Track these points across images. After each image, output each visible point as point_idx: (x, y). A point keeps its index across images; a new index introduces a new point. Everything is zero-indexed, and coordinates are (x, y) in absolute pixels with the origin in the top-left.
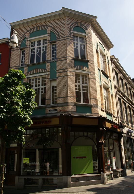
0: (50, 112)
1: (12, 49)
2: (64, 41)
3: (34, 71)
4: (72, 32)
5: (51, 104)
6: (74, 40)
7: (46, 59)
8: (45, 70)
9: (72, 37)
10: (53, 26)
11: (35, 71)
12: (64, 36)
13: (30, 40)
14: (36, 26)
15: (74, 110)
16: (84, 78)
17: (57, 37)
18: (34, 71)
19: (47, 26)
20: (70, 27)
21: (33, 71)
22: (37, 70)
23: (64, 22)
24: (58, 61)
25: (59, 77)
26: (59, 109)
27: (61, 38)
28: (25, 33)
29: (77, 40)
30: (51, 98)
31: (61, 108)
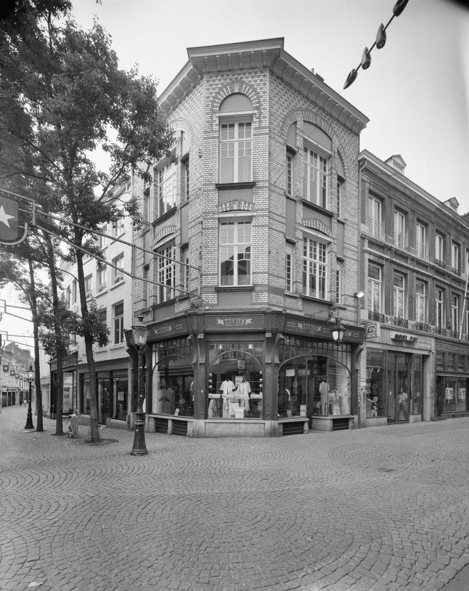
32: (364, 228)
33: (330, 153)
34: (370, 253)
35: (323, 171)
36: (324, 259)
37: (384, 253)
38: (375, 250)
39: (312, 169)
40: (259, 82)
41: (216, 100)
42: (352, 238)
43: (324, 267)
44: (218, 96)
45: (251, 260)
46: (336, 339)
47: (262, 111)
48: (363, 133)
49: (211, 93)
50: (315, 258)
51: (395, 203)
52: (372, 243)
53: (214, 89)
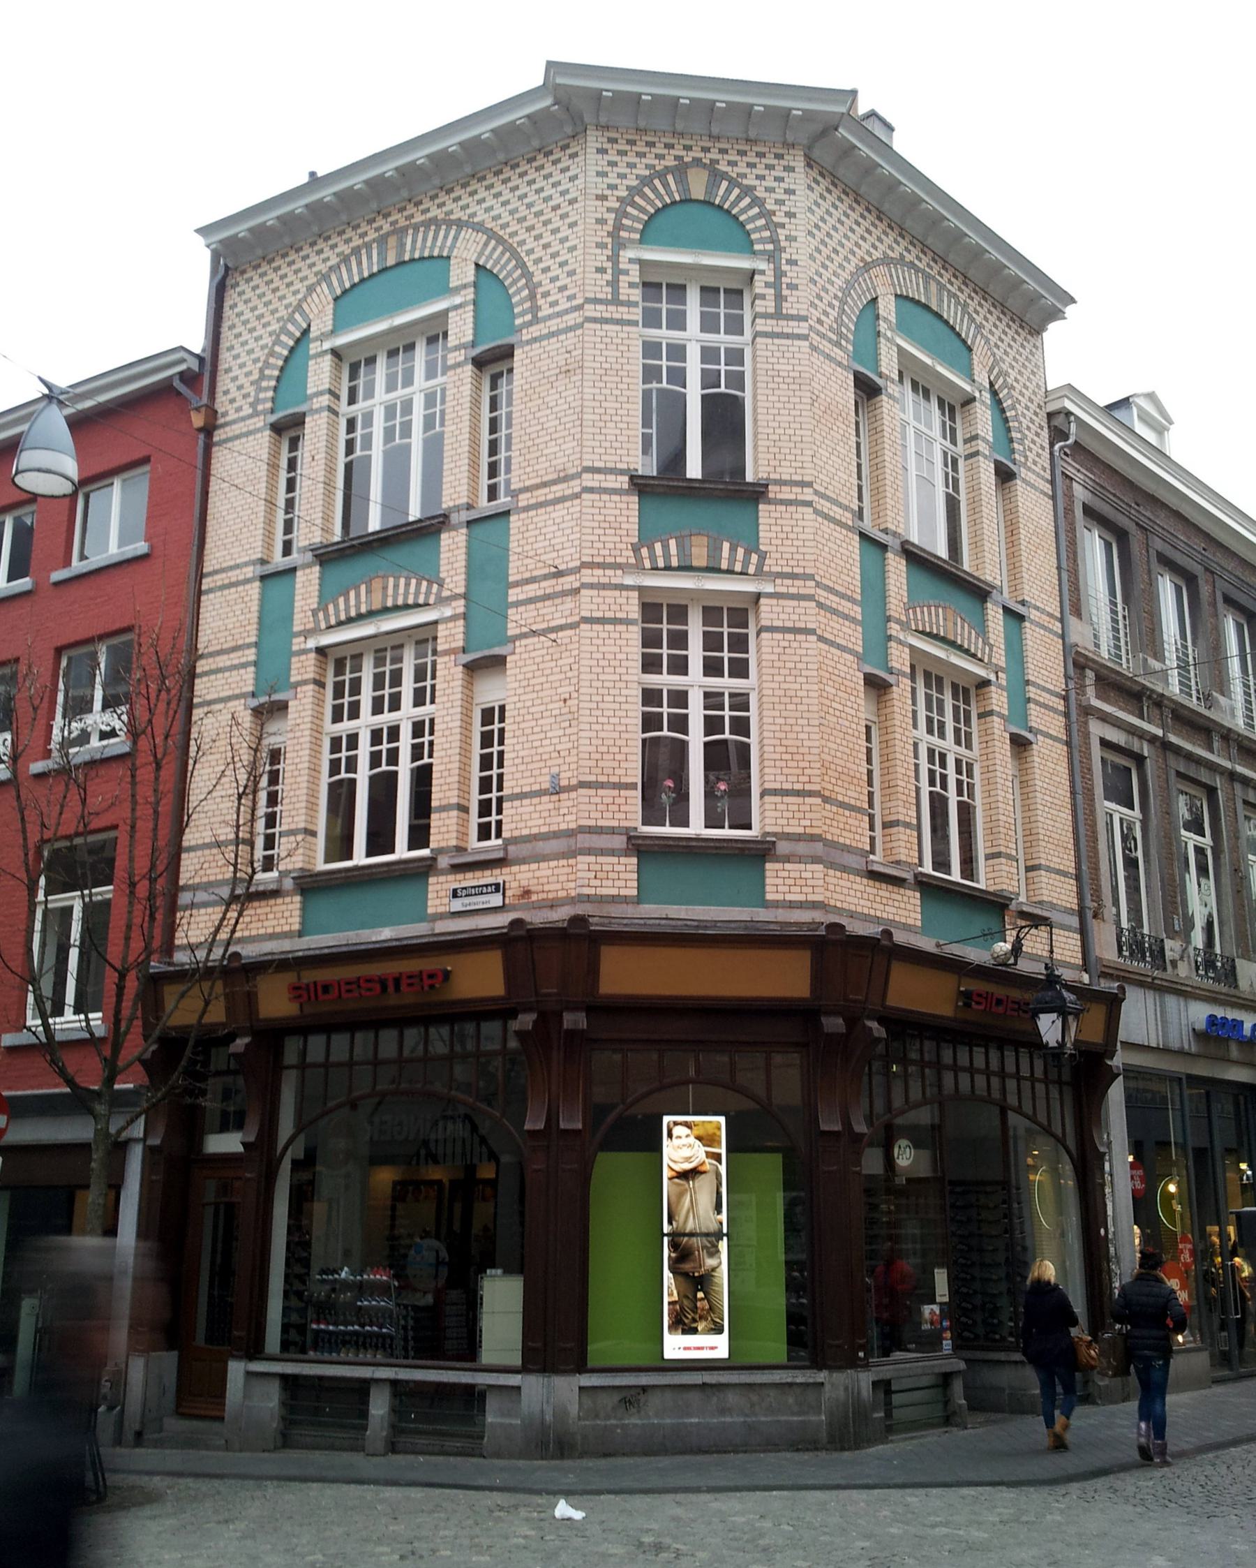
0: (457, 905)
1: (215, 427)
2: (570, 339)
3: (358, 596)
4: (631, 261)
5: (474, 843)
6: (651, 319)
7: (441, 496)
8: (435, 586)
9: (629, 304)
10: (494, 219)
11: (369, 592)
12: (569, 298)
13: (335, 353)
14: (377, 230)
15: (622, 883)
16: (726, 630)
17: (523, 314)
18: (363, 598)
19: (450, 224)
20: (621, 214)
21: (341, 600)
22: (377, 584)
23: (576, 177)
24: (527, 509)
25: (524, 636)
26: (516, 877)
27: (550, 317)
28: (305, 298)
29: (678, 321)
30: (475, 797)
31: (530, 875)
32: (1079, 633)
33: (968, 388)
34: (1105, 718)
35: (948, 443)
36: (968, 735)
37: (1141, 717)
38: (1121, 708)
39: (918, 434)
40: (760, 170)
41: (629, 209)
42: (1045, 665)
43: (970, 767)
44: (637, 199)
45: (753, 741)
46: (1053, 1044)
47: (785, 268)
48: (1053, 331)
49: (613, 187)
50: (942, 735)
51: (1158, 544)
52: (1111, 684)
53: (622, 176)
